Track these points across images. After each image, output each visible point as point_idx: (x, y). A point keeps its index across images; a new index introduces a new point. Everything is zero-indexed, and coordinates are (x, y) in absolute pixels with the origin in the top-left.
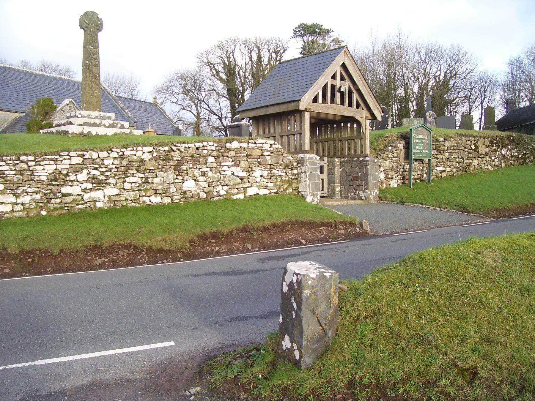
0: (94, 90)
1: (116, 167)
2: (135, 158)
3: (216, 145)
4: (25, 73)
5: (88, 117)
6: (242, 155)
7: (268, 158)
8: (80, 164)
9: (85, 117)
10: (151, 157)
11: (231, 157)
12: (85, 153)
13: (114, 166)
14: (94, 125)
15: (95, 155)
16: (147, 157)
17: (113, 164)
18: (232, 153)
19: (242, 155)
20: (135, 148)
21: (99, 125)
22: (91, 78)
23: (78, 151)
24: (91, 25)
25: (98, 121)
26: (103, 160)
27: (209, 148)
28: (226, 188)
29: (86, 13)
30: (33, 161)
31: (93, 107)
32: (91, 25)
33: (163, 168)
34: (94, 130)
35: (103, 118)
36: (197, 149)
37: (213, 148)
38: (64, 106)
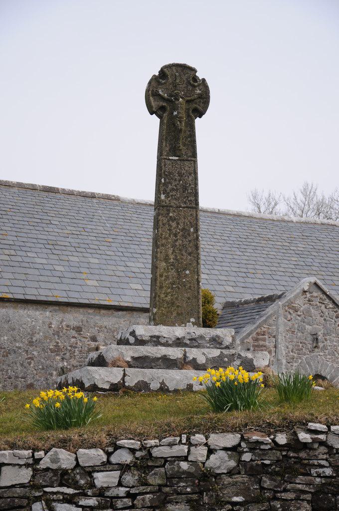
1: (129, 495)
2: (184, 465)
4: (262, 222)
5: (156, 341)
8: (22, 486)
12: (39, 454)
13: (122, 491)
14: (168, 363)
15: (66, 459)
16: (220, 462)
17: (120, 484)
20: (184, 437)
23: (19, 448)
24: (178, 98)
25: (175, 353)
26: (90, 474)
29: (163, 73)
30: (196, 445)
32: (178, 98)
33: (275, 498)
34: (155, 376)
35: (194, 342)
38: (296, 297)
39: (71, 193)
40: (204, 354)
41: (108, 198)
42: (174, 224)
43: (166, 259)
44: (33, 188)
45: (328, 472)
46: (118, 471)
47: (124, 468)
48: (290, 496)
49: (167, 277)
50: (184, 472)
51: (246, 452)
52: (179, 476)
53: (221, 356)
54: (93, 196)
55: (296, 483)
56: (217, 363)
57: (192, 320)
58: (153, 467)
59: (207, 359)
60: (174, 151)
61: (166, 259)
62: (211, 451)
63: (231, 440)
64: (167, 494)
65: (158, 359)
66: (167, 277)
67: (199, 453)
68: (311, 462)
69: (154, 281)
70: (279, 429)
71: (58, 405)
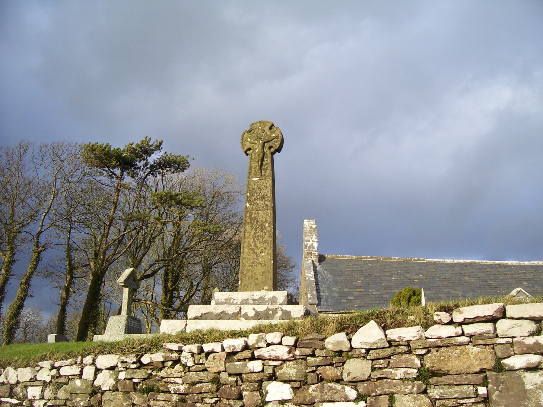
0: (258, 251)
3: (290, 340)
6: (400, 373)
9: (222, 304)
10: (112, 382)
11: (354, 383)
16: (105, 381)
18: (356, 368)
19: (400, 373)
21: (236, 316)
22: (254, 231)
27: (265, 352)
31: (256, 284)
36: (231, 355)
37: (282, 352)
40: (254, 309)
46: (39, 387)
47: (45, 384)
50: (79, 388)
51: (122, 371)
55: (157, 400)
57: (266, 288)
62: (98, 371)
67: (88, 373)
68: (169, 379)
69: (472, 304)
71: (155, 350)
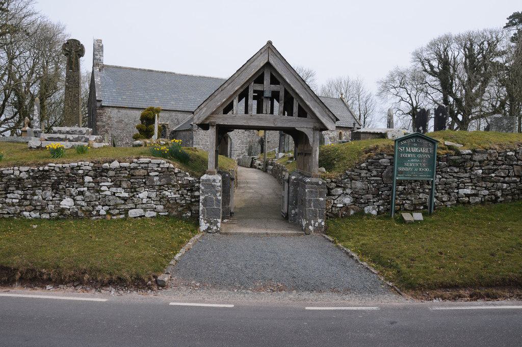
2: (12, 176)
7: (156, 179)
28: (107, 208)
39: (158, 72)
41: (171, 73)
42: (71, 93)
43: (68, 105)
44: (145, 70)
45: (56, 178)
48: (45, 185)
49: (68, 111)
52: (10, 179)
53: (78, 137)
54: (165, 72)
56: (77, 140)
58: (4, 177)
59: (73, 138)
60: (71, 68)
61: (68, 105)
62: (21, 172)
63: (26, 168)
64: (9, 184)
65: (57, 138)
66: (68, 111)
67: (17, 173)
70: (42, 165)
